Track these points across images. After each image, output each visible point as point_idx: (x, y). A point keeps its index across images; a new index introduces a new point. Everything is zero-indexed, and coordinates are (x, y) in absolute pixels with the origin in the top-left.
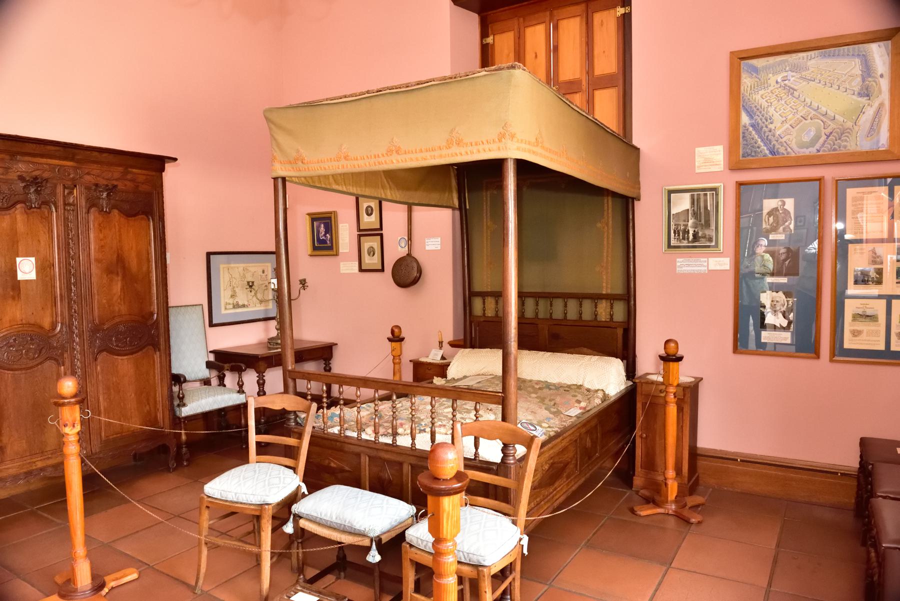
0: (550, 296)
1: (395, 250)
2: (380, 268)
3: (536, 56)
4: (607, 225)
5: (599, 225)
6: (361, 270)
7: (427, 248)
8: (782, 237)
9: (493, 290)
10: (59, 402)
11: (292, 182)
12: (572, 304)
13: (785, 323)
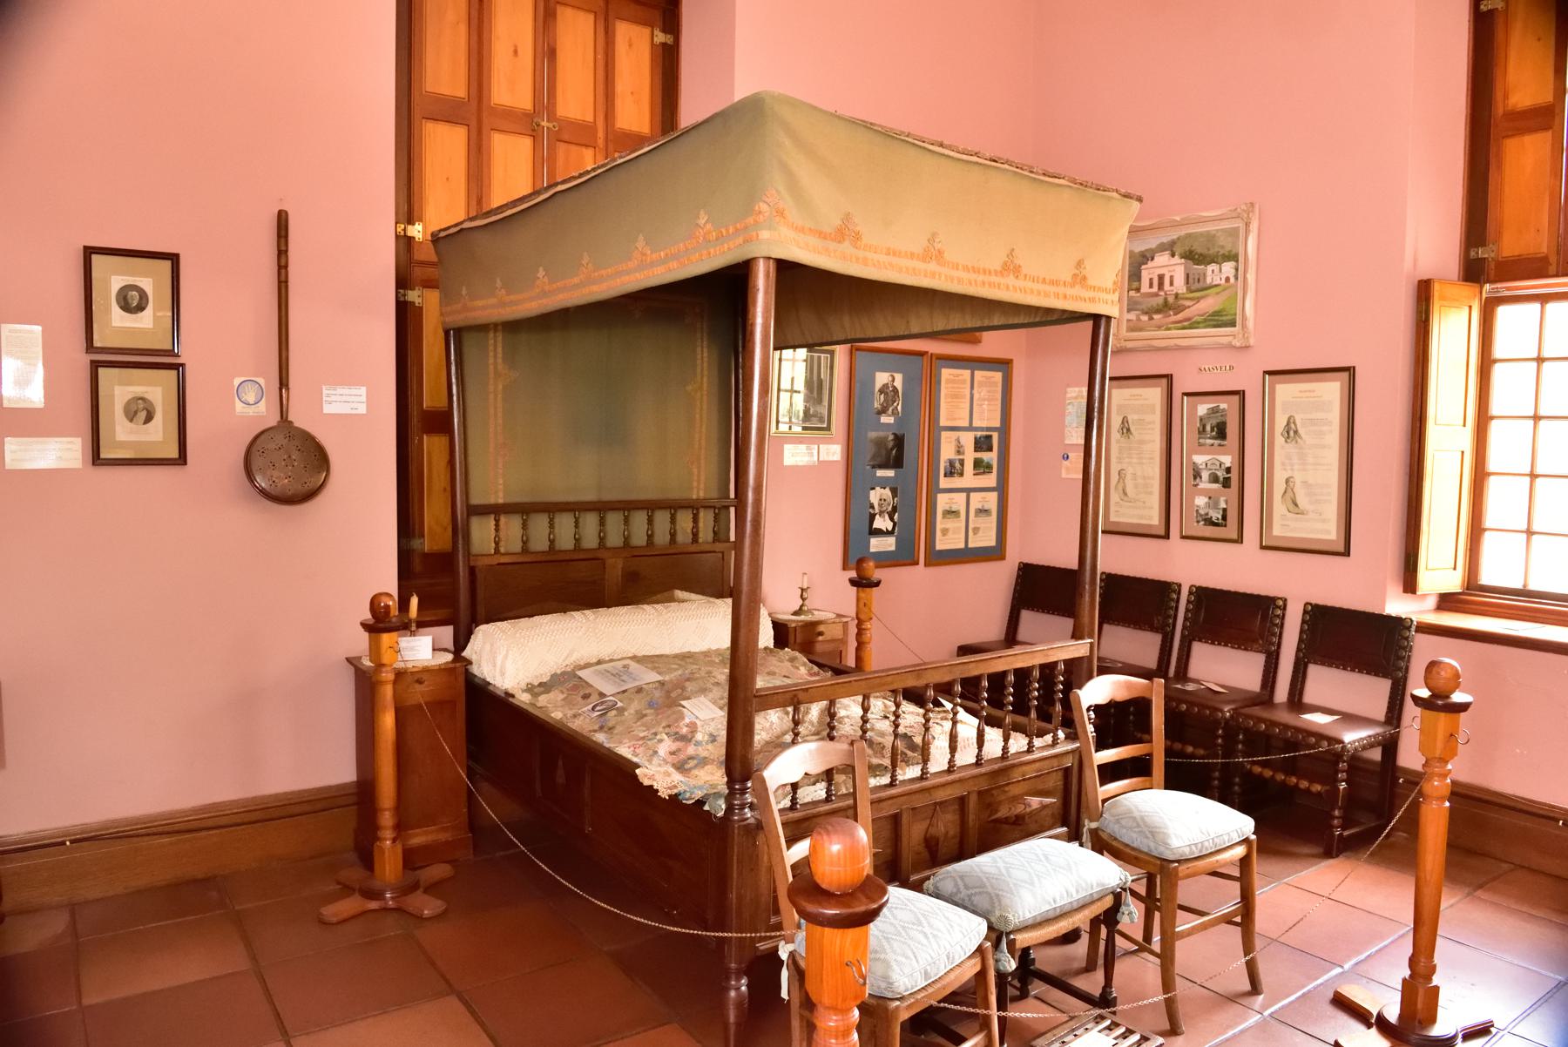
0: (627, 507)
1: (235, 404)
2: (174, 454)
3: (516, 52)
4: (701, 388)
5: (689, 388)
6: (96, 458)
7: (327, 409)
8: (891, 420)
9: (509, 500)
10: (1334, 818)
11: (479, 201)
12: (590, 521)
13: (890, 526)
